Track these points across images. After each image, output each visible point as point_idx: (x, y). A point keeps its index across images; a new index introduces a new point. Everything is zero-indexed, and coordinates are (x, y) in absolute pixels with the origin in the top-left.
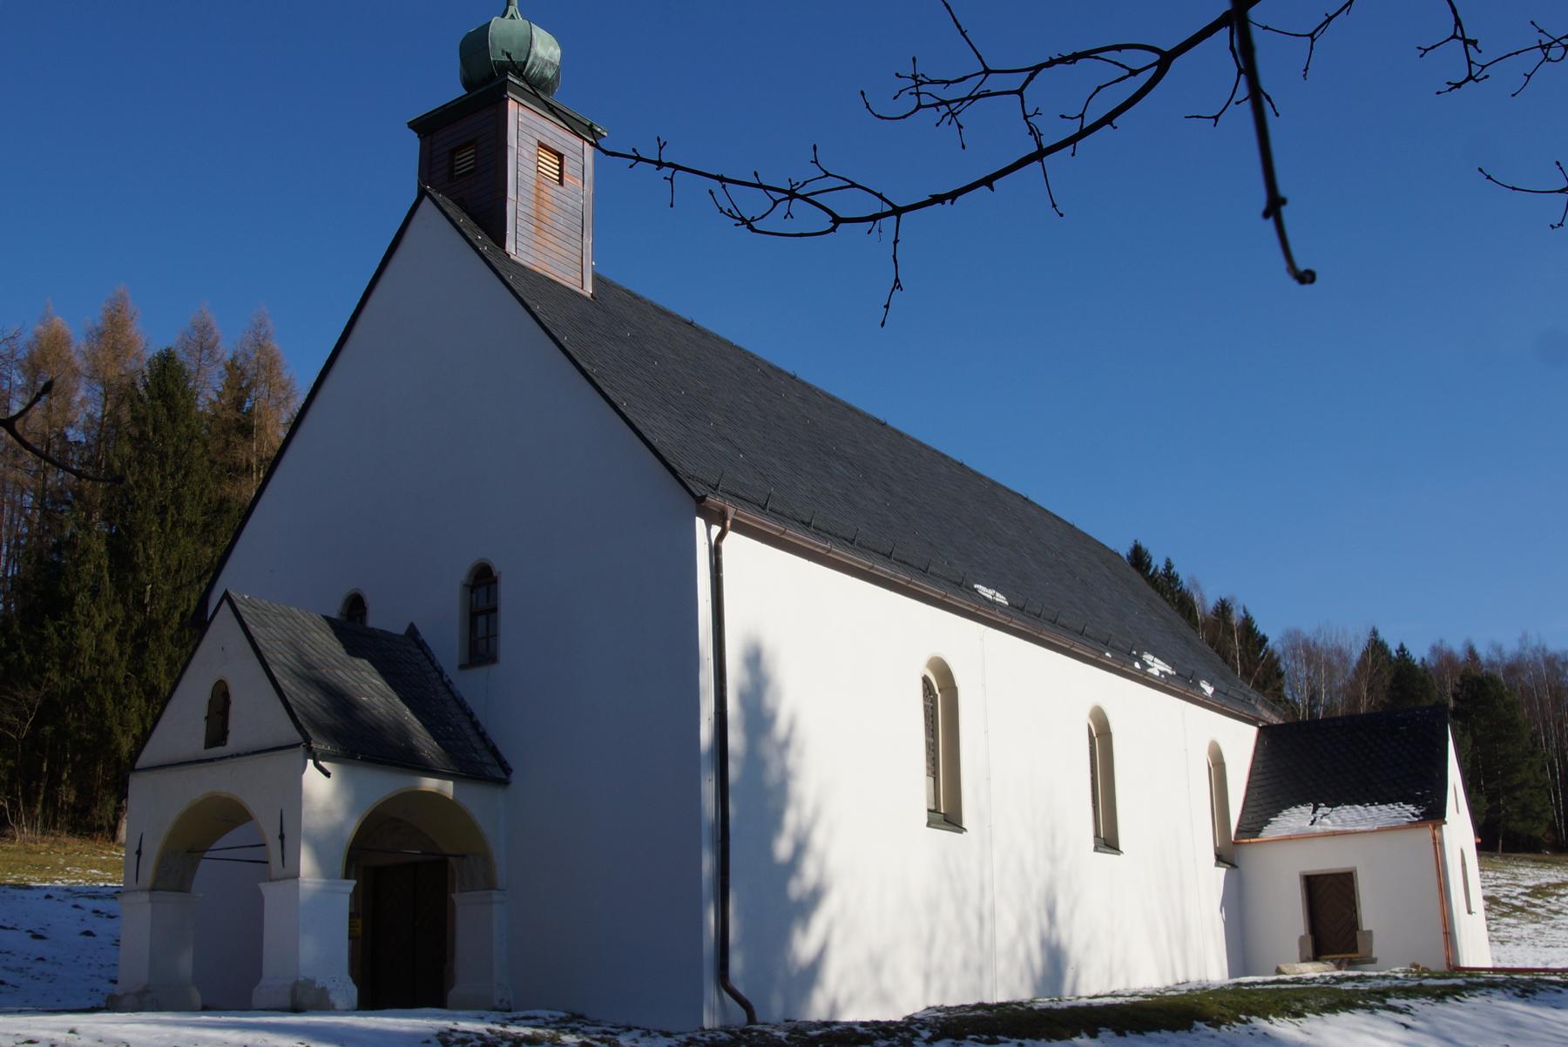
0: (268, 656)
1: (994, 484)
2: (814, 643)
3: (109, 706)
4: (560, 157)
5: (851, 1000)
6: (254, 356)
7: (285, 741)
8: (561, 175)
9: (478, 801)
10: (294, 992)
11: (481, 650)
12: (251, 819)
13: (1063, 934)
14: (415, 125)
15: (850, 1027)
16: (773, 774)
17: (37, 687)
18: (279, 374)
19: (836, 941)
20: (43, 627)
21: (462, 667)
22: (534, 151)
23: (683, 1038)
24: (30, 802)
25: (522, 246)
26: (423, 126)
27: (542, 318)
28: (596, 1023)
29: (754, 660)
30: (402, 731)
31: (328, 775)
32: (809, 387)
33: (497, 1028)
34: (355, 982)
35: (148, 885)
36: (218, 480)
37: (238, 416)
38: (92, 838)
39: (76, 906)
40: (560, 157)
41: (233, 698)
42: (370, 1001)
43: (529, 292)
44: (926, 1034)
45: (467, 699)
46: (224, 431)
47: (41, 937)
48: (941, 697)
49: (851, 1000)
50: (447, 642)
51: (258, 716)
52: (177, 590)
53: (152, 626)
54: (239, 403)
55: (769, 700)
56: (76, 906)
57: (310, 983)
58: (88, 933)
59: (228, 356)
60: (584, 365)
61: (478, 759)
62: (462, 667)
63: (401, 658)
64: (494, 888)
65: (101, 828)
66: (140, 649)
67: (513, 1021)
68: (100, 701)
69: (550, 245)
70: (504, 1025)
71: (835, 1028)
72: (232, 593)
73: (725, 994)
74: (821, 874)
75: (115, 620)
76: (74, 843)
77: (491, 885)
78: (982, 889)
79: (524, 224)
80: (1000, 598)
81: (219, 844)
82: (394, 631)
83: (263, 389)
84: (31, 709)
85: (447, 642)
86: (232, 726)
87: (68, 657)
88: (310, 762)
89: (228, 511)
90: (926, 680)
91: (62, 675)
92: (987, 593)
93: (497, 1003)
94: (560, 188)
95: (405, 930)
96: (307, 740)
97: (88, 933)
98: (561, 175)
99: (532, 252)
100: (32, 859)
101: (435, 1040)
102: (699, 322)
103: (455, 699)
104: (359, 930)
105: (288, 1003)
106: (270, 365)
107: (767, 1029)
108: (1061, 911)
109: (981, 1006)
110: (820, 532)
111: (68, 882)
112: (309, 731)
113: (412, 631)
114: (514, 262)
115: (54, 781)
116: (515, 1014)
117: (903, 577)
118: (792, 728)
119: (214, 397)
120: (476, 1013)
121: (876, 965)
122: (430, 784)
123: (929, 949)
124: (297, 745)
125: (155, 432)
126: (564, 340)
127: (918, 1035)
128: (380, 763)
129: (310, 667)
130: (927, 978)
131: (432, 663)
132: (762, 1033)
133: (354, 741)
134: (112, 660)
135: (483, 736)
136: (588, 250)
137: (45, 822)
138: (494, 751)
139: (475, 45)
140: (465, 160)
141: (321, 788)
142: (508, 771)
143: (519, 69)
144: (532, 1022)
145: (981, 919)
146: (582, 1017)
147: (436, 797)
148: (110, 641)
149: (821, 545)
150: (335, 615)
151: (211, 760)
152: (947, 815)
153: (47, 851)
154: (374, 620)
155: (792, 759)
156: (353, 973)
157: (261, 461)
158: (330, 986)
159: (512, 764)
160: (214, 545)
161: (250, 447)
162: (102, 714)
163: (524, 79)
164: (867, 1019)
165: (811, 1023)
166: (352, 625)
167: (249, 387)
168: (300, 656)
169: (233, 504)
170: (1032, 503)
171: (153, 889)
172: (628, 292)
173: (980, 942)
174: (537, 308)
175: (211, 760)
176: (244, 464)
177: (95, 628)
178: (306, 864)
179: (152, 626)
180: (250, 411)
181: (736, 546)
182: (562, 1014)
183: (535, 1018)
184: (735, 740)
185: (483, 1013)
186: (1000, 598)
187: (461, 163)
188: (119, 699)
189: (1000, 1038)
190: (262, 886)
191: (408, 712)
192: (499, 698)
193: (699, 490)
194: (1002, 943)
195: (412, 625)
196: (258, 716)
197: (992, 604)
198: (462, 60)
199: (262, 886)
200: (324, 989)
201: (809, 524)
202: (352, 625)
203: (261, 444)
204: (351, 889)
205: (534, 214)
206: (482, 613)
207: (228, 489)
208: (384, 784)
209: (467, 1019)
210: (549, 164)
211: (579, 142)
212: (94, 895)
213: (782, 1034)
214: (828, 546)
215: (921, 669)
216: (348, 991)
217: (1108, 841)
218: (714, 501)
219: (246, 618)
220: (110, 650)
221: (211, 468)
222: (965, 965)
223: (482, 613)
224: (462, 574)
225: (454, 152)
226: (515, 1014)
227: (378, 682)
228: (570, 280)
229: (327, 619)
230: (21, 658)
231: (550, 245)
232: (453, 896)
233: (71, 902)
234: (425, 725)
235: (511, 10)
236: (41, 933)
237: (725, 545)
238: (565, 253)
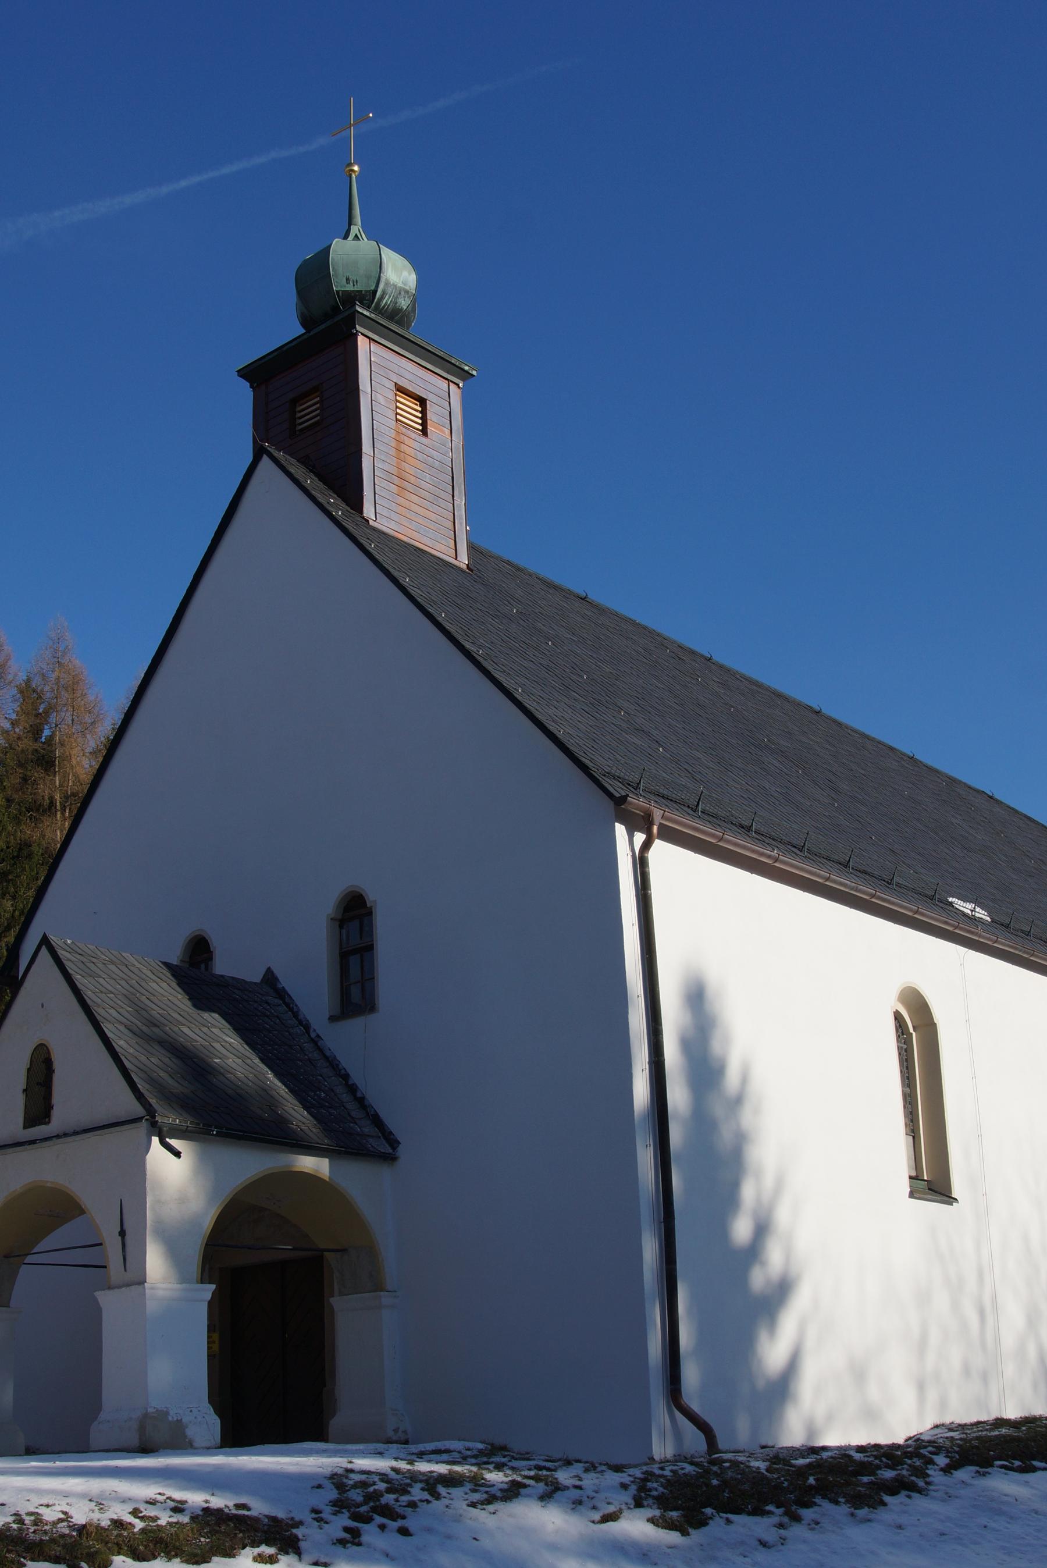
0: (99, 1012)
1: (953, 781)
2: (762, 971)
4: (422, 402)
5: (830, 1418)
6: (53, 677)
7: (122, 1114)
8: (424, 424)
9: (358, 1182)
10: (142, 1429)
12: (82, 1212)
14: (246, 373)
15: (843, 1453)
16: (726, 1134)
18: (84, 695)
19: (810, 1344)
21: (333, 1019)
22: (391, 396)
23: (638, 1473)
25: (384, 509)
26: (256, 374)
27: (414, 592)
28: (525, 1456)
29: (697, 997)
30: (270, 1101)
31: (177, 1154)
32: (728, 671)
33: (403, 1465)
36: (17, 820)
37: (37, 746)
40: (422, 402)
41: (56, 1065)
42: (235, 1437)
43: (392, 563)
44: (942, 1460)
46: (21, 765)
48: (917, 1035)
49: (830, 1418)
50: (312, 989)
51: (87, 1084)
54: (36, 732)
55: (716, 1046)
57: (164, 1414)
59: (22, 677)
60: (467, 645)
61: (360, 1132)
62: (333, 1019)
63: (260, 1010)
67: (421, 1455)
69: (415, 508)
70: (411, 1463)
71: (825, 1455)
72: (53, 938)
73: (678, 1415)
77: (377, 1286)
79: (385, 484)
80: (981, 914)
81: (41, 1246)
85: (312, 989)
86: (56, 1099)
88: (155, 1140)
89: (30, 856)
90: (898, 1016)
93: (390, 1434)
94: (423, 439)
95: (275, 1341)
96: (151, 1112)
98: (424, 424)
99: (393, 516)
101: (328, 1484)
102: (592, 596)
103: (326, 1058)
104: (216, 1347)
105: (135, 1442)
106: (73, 685)
107: (741, 1458)
109: (1000, 1422)
110: (766, 838)
112: (153, 1101)
113: (270, 978)
114: (374, 529)
116: (421, 1447)
117: (865, 891)
118: (745, 1079)
120: (372, 1446)
121: (859, 1373)
123: (922, 1346)
124: (138, 1120)
126: (442, 617)
127: (931, 1462)
128: (239, 1138)
129: (153, 1023)
130: (921, 1387)
131: (296, 1015)
132: (735, 1464)
133: (214, 1114)
135: (361, 1102)
136: (461, 513)
138: (377, 1121)
139: (314, 273)
140: (309, 411)
141: (175, 1175)
142: (394, 1143)
143: (368, 297)
144: (445, 1457)
146: (504, 1448)
147: (310, 1179)
149: (766, 854)
150: (175, 961)
151: (33, 1142)
152: (933, 1183)
154: (223, 966)
155: (747, 1118)
156: (211, 1401)
157: (66, 797)
159: (399, 1135)
160: (14, 898)
161: (53, 782)
163: (379, 310)
164: (863, 1442)
165: (793, 1449)
166: (195, 970)
167: (47, 712)
168: (139, 1010)
169: (34, 848)
170: (998, 802)
172: (509, 563)
174: (406, 581)
175: (33, 1142)
176: (47, 801)
178: (156, 1263)
180: (51, 738)
181: (667, 858)
182: (480, 1446)
183: (447, 1451)
184: (677, 1096)
185: (381, 1446)
186: (981, 914)
187: (304, 410)
189: (1036, 1463)
190: (99, 1295)
191: (270, 1075)
193: (618, 790)
195: (269, 971)
196: (87, 1084)
198: (299, 292)
199: (99, 1295)
200: (179, 1421)
201: (749, 829)
202: (195, 970)
203: (65, 777)
204: (208, 1296)
205: (394, 471)
206: (354, 952)
207: (28, 831)
208: (251, 1164)
209: (364, 1454)
210: (410, 411)
211: (444, 384)
213: (762, 1465)
214: (775, 853)
215: (890, 1003)
218: (637, 802)
219: (68, 965)
221: (9, 807)
222: (967, 1370)
223: (354, 952)
224: (328, 904)
225: (295, 402)
226: (421, 1447)
227: (233, 1040)
228: (439, 546)
229: (166, 964)
231: (415, 508)
232: (331, 1300)
234: (291, 1091)
235: (354, 230)
237: (652, 855)
238: (433, 517)
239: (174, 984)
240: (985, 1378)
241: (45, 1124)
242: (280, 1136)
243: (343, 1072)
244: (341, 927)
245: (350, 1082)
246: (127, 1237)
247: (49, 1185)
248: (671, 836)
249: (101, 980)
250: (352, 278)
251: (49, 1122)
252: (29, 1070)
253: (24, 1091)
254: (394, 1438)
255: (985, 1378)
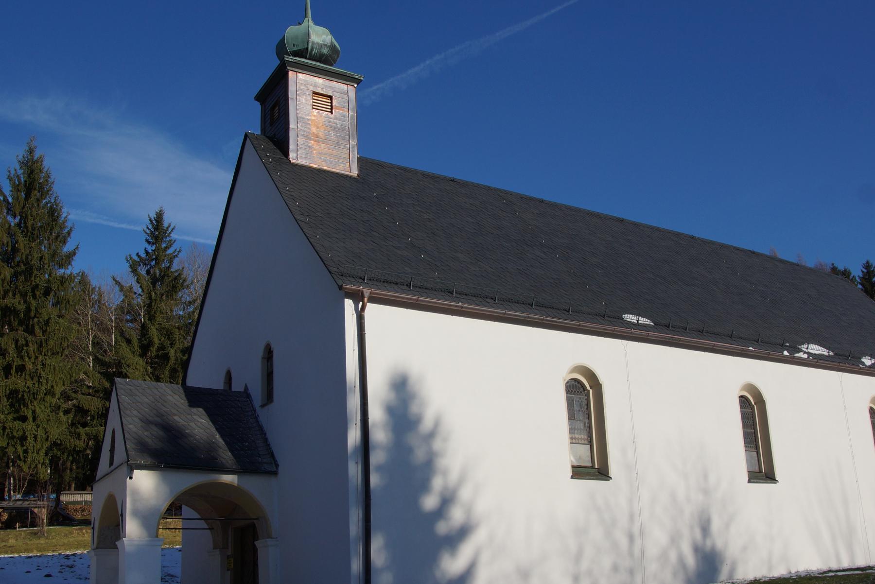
9: (255, 486)
11: (269, 397)
13: (718, 540)
16: (420, 455)
19: (484, 559)
22: (310, 98)
29: (401, 386)
40: (331, 97)
55: (414, 409)
58: (48, 576)
74: (469, 511)
78: (631, 518)
80: (643, 321)
92: (630, 318)
97: (48, 576)
108: (716, 525)
118: (437, 424)
122: (228, 479)
141: (145, 484)
145: (631, 538)
152: (595, 469)
155: (437, 444)
173: (631, 554)
186: (643, 321)
192: (282, 424)
194: (653, 551)
197: (637, 325)
208: (190, 480)
217: (763, 472)
222: (615, 568)
234: (226, 443)
237: (367, 314)
239: (183, 396)
240: (631, 572)
242: (214, 466)
248: (374, 300)
249: (137, 398)
250: (296, 44)
255: (631, 572)
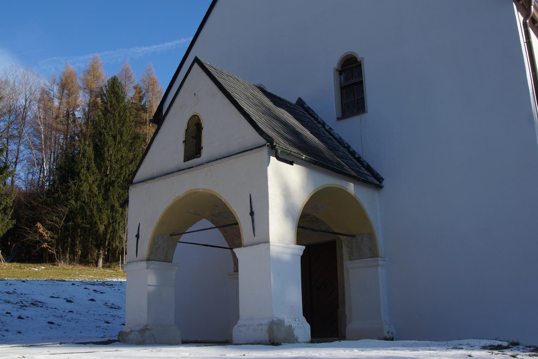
3: (95, 212)
10: (270, 330)
17: (66, 206)
20: (68, 182)
21: (339, 119)
24: (64, 254)
34: (308, 321)
35: (145, 257)
38: (88, 266)
39: (86, 288)
41: (204, 125)
45: (344, 138)
47: (71, 302)
52: (121, 168)
53: (112, 183)
56: (86, 288)
58: (92, 300)
62: (339, 119)
64: (378, 257)
65: (92, 262)
66: (107, 190)
68: (91, 211)
75: (97, 180)
76: (81, 267)
77: (374, 254)
82: (288, 99)
83: (150, 94)
84: (64, 215)
87: (78, 195)
91: (76, 201)
97: (92, 300)
100: (66, 272)
111: (81, 280)
115: (73, 245)
119: (130, 99)
120: (393, 348)
125: (110, 107)
131: (316, 119)
134: (96, 195)
137: (70, 260)
142: (380, 179)
148: (95, 189)
153: (72, 269)
156: (305, 314)
158: (294, 325)
159: (382, 174)
162: (92, 216)
171: (148, 260)
177: (89, 183)
179: (112, 183)
188: (100, 210)
196: (223, 129)
200: (290, 326)
212: (93, 284)
216: (303, 329)
220: (95, 191)
224: (335, 62)
230: (59, 196)
233: (83, 286)
236: (71, 300)
241: (198, 157)
243: (346, 145)
244: (340, 74)
245: (351, 150)
246: (255, 216)
247: (201, 190)
251: (200, 156)
252: (186, 130)
253: (184, 142)
254: (388, 336)
